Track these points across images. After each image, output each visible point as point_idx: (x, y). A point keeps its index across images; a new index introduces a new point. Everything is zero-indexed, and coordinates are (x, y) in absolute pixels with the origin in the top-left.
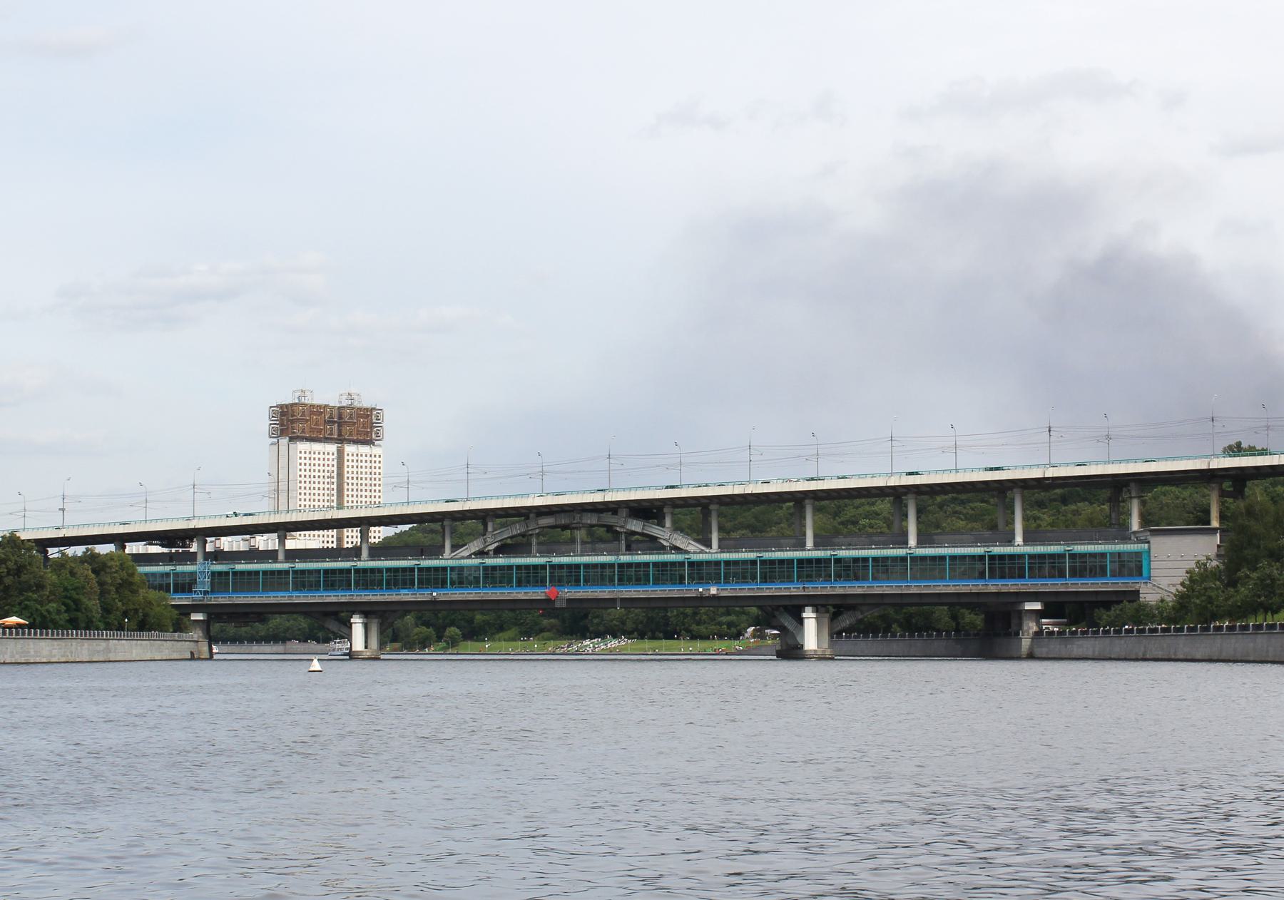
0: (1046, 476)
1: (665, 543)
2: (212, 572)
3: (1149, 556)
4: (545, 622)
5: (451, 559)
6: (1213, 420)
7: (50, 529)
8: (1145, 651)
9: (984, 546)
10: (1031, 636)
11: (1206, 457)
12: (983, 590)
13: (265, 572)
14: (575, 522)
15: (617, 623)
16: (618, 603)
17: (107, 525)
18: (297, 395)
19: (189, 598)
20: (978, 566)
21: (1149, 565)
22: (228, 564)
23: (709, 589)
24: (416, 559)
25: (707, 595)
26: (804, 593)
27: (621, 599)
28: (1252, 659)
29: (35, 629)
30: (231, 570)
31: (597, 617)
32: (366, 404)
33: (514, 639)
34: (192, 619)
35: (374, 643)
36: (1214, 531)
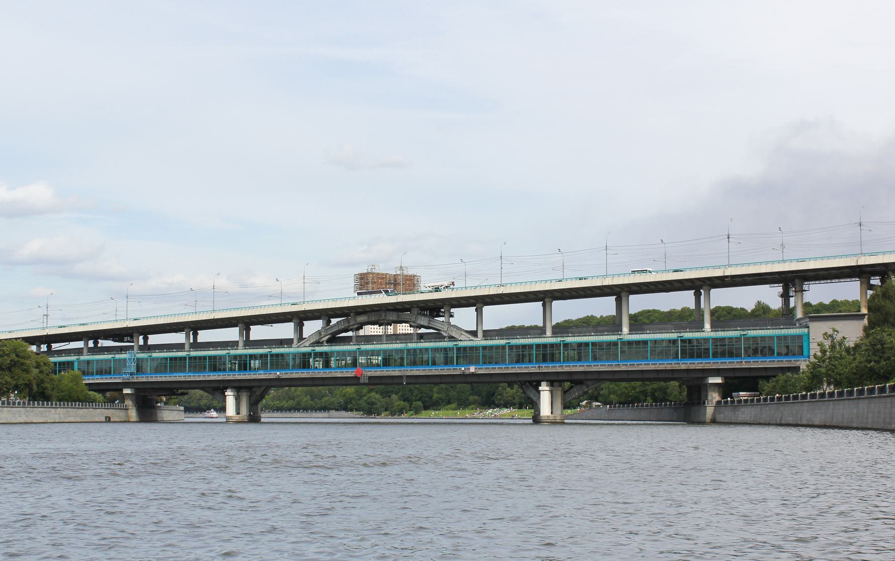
0: (725, 275)
1: (444, 334)
2: (137, 359)
3: (809, 338)
4: (471, 398)
5: (298, 347)
6: (861, 225)
7: (40, 329)
8: (782, 417)
9: (677, 332)
10: (714, 405)
11: (856, 255)
12: (675, 367)
13: (171, 359)
14: (382, 319)
15: (511, 399)
16: (405, 379)
17: (469, 289)
18: (370, 268)
19: (121, 378)
20: (673, 349)
21: (809, 345)
22: (148, 353)
23: (469, 369)
24: (269, 348)
25: (468, 373)
26: (539, 371)
27: (407, 376)
28: (855, 425)
29: (110, 403)
30: (312, 351)
31: (500, 395)
32: (411, 272)
33: (455, 409)
34: (124, 392)
35: (244, 411)
36: (864, 315)
